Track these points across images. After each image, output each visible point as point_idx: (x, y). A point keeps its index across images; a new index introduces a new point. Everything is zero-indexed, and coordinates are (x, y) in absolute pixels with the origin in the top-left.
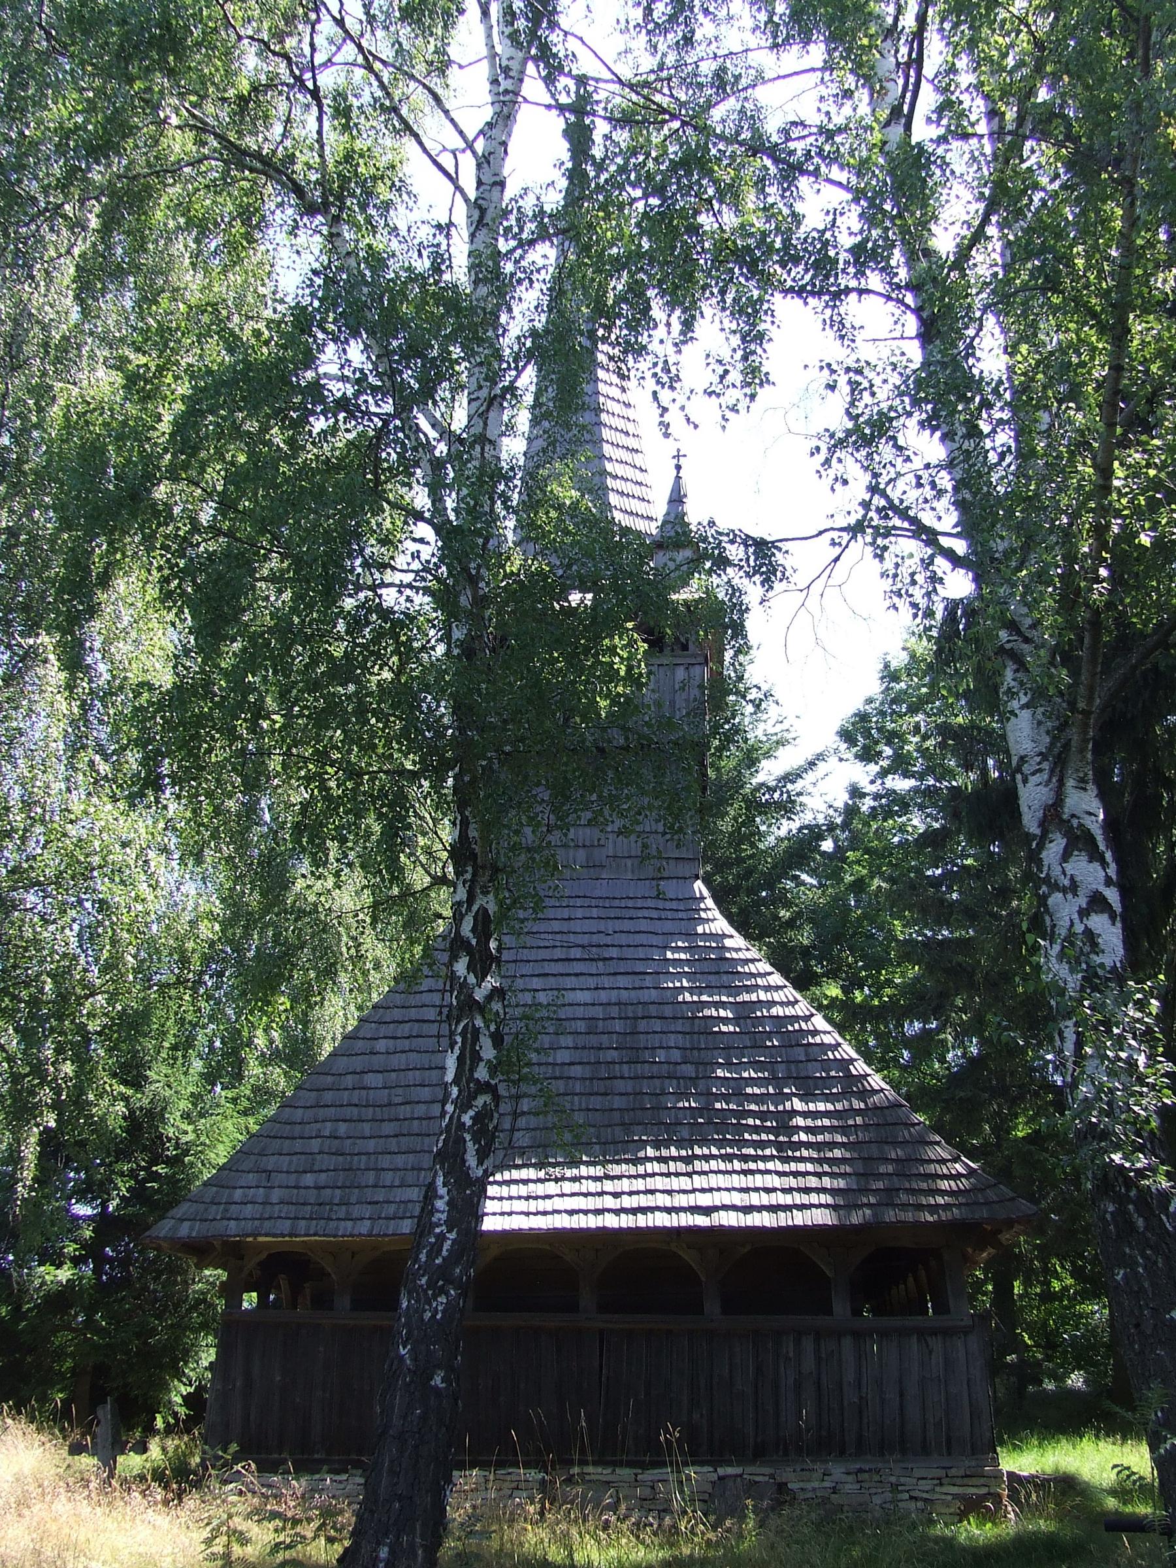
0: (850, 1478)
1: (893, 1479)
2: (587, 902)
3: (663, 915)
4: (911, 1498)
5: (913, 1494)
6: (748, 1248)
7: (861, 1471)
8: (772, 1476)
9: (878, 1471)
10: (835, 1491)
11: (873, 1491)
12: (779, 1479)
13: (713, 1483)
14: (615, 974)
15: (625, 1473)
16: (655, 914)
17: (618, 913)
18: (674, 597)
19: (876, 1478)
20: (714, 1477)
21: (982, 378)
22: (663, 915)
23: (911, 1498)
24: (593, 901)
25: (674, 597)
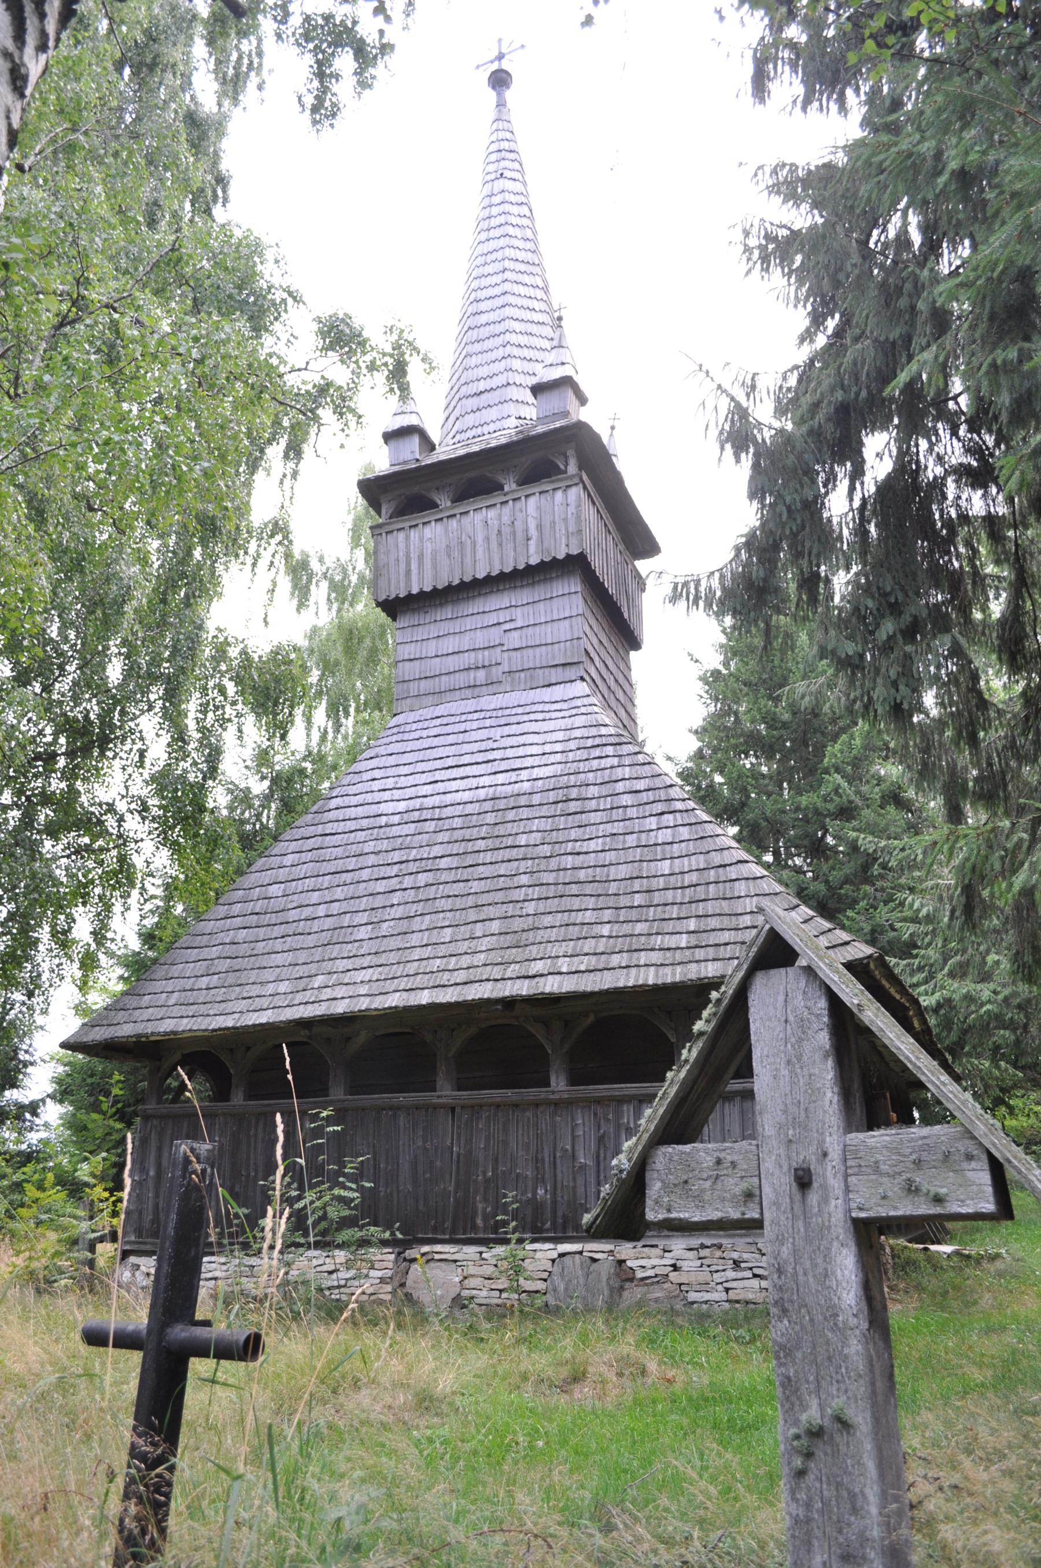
0: (692, 1255)
1: (735, 1255)
2: (482, 715)
3: (548, 716)
4: (755, 1276)
5: (757, 1271)
6: (591, 1018)
7: (703, 1246)
8: (611, 1252)
9: (719, 1247)
10: (675, 1268)
11: (714, 1268)
12: (619, 1257)
13: (553, 1261)
14: (496, 773)
15: (471, 1250)
16: (540, 716)
17: (503, 721)
18: (975, 464)
19: (718, 1253)
20: (554, 1255)
21: (1000, 652)
22: (548, 716)
23: (755, 1276)
24: (488, 714)
25: (975, 464)
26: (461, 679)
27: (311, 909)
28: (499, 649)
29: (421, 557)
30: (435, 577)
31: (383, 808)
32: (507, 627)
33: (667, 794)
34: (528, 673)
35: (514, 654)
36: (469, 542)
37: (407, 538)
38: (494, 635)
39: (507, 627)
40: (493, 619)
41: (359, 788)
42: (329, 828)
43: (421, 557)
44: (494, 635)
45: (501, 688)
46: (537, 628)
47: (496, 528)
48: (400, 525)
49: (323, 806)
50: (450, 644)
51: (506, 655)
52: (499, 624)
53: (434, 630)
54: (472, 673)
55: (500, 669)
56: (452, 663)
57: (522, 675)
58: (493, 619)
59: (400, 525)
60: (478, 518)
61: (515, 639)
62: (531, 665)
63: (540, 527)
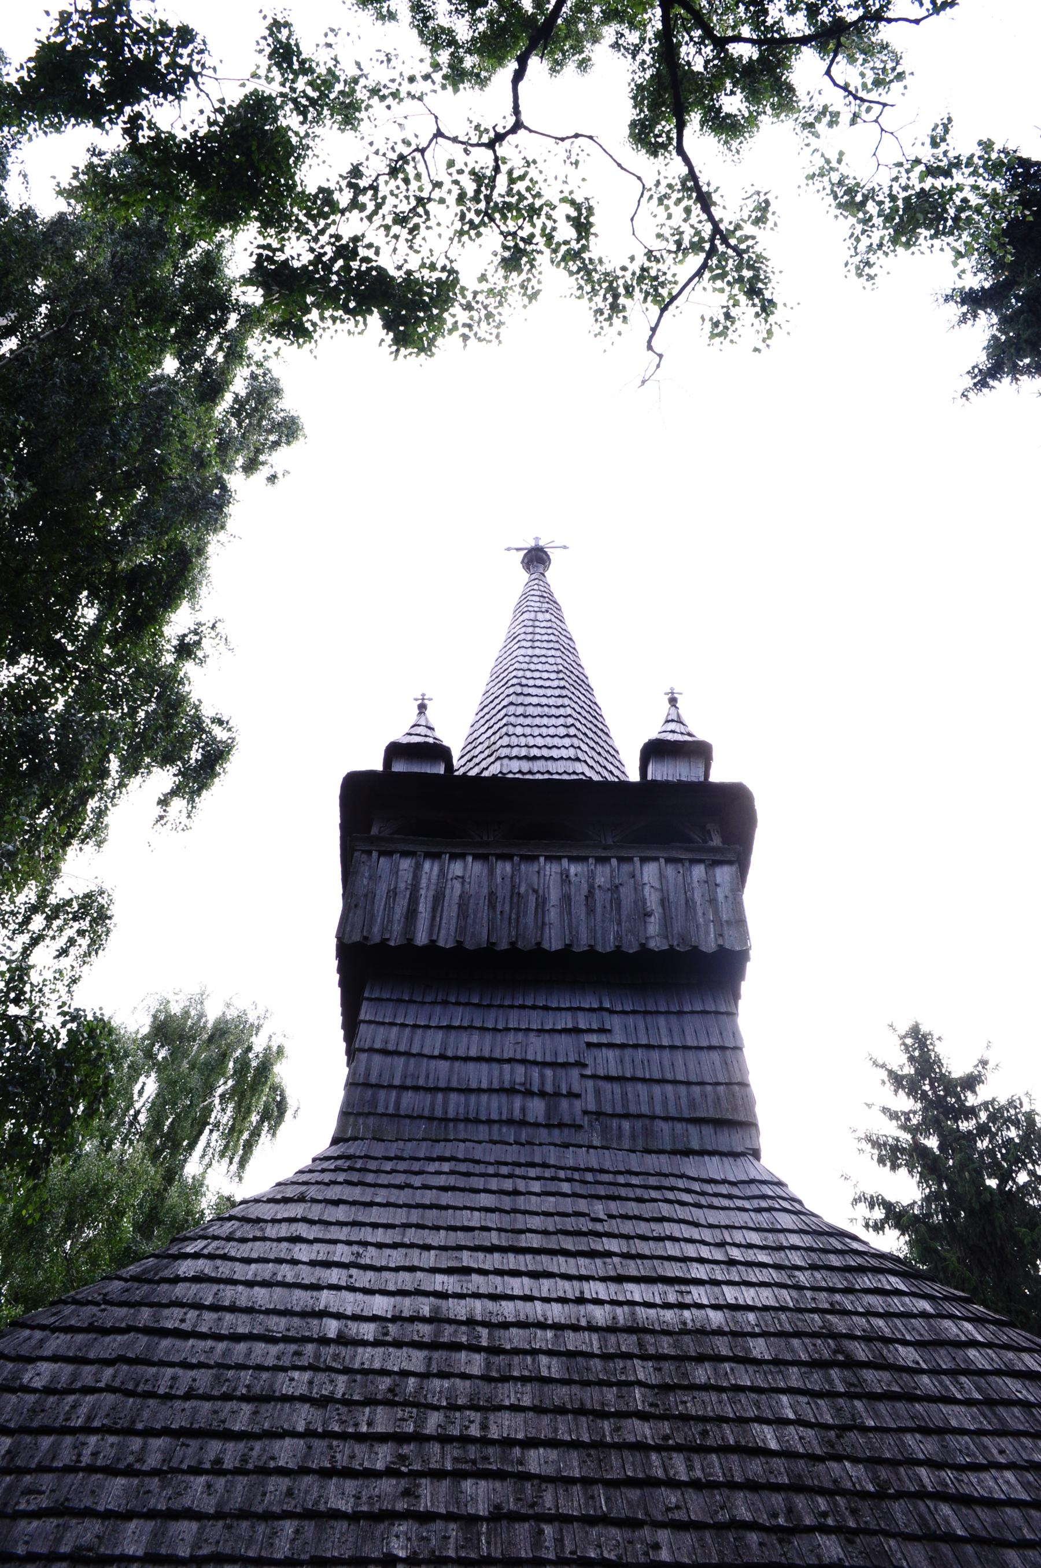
26: (494, 1106)
27: (96, 1526)
28: (575, 1073)
29: (438, 899)
30: (461, 929)
31: (326, 1299)
32: (594, 1038)
33: (456, 1494)
34: (639, 1124)
35: (606, 1086)
36: (532, 898)
37: (418, 867)
38: (566, 1048)
39: (594, 1038)
40: (565, 1021)
41: (257, 1250)
42: (172, 1318)
43: (438, 899)
44: (566, 1048)
45: (581, 1138)
46: (655, 1055)
47: (584, 891)
48: (411, 848)
49: (157, 1269)
50: (473, 1044)
51: (590, 1084)
52: (576, 1031)
53: (459, 1017)
54: (518, 1102)
55: (578, 1105)
56: (479, 1075)
57: (626, 1125)
58: (565, 1021)
59: (411, 848)
60: (552, 870)
61: (608, 1062)
62: (645, 1109)
63: (664, 902)
